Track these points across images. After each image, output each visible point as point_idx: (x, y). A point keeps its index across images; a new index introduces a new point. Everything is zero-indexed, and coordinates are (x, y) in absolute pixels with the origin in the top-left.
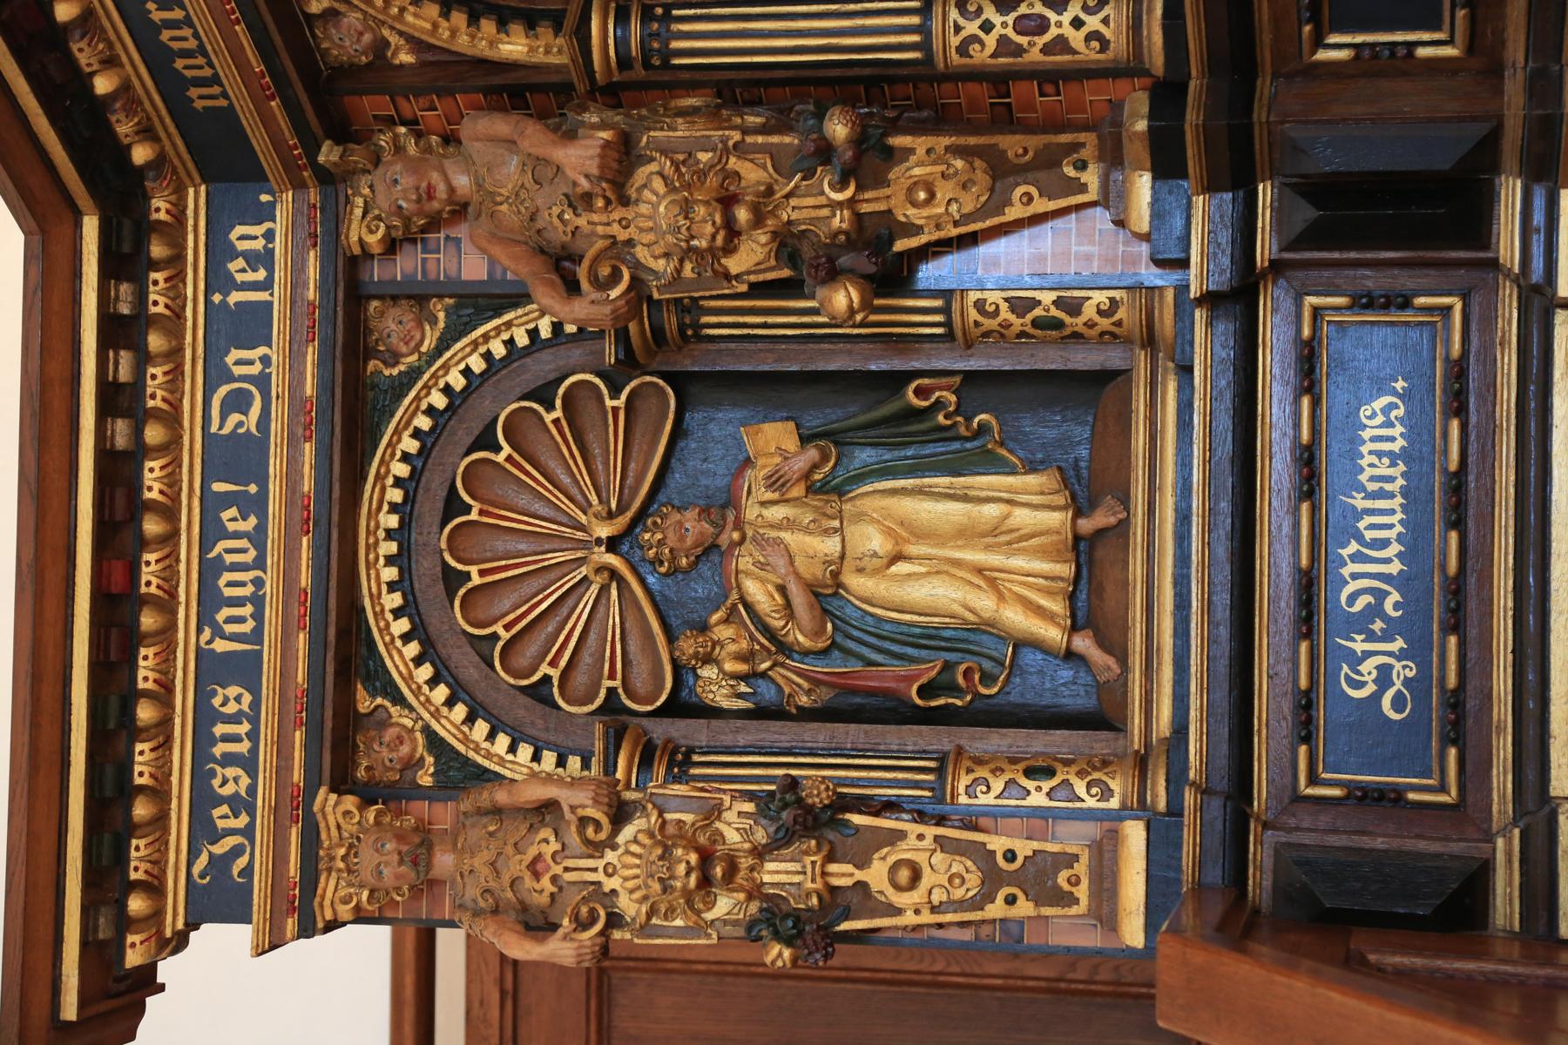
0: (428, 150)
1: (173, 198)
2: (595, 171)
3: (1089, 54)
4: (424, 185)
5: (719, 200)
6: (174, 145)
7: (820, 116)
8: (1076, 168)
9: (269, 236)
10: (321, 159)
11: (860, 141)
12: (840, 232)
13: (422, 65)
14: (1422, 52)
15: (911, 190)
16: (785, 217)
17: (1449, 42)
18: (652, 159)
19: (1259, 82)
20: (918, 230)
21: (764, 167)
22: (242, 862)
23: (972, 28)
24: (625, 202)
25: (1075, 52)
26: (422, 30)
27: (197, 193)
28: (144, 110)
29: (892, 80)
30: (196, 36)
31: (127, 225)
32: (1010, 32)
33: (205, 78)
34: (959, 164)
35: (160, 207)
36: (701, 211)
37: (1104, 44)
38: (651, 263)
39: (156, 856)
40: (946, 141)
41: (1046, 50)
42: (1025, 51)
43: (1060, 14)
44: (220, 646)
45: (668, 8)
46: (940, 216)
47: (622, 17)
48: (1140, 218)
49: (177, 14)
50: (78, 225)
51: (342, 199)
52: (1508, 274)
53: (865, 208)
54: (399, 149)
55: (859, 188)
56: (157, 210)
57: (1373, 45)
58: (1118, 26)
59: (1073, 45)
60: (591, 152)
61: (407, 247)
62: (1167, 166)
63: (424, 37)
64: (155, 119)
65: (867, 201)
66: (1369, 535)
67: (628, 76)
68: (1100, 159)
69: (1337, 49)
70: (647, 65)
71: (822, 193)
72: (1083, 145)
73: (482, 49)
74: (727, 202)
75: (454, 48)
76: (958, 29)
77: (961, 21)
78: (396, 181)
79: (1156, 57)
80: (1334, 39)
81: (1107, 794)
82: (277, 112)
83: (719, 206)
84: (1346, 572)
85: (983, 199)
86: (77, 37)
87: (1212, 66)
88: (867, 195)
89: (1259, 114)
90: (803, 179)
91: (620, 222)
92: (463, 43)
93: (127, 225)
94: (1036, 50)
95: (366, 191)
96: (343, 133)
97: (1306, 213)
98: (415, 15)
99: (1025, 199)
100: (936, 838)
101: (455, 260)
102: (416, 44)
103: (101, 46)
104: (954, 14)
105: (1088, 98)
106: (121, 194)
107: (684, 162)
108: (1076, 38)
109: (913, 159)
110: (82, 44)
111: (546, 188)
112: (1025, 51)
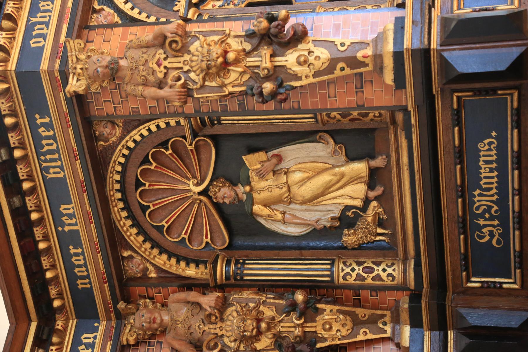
0: (156, 307)
1: (64, 322)
2: (213, 305)
3: (388, 282)
4: (152, 317)
5: (256, 319)
6: (69, 302)
7: (293, 294)
8: (383, 325)
9: (95, 338)
10: (118, 306)
11: (306, 302)
12: (297, 336)
13: (158, 278)
14: (505, 286)
15: (324, 325)
16: (278, 330)
17: (515, 283)
18: (234, 305)
19: (448, 293)
20: (325, 340)
21: (273, 311)
23: (348, 270)
24: (222, 320)
25: (383, 281)
26: (160, 264)
27: (73, 322)
28: (61, 287)
29: (319, 287)
30: (84, 259)
31: (47, 329)
32: (361, 272)
33: (84, 276)
34: (341, 317)
35: (59, 324)
36: (249, 322)
37: (394, 278)
38: (229, 344)
40: (336, 308)
41: (373, 279)
42: (366, 279)
43: (378, 267)
45: (244, 260)
46: (334, 335)
47: (228, 263)
48: (406, 341)
49: (79, 251)
50: (29, 325)
51: (123, 325)
53: (307, 330)
54: (146, 306)
55: (305, 322)
56: (58, 325)
57: (487, 282)
58: (398, 271)
59: (383, 278)
60: (212, 299)
61: (143, 344)
62: (416, 323)
63: (161, 266)
64: (64, 291)
65: (308, 327)
66: (484, 186)
67: (228, 282)
68: (392, 322)
69: (475, 283)
70: (235, 279)
71: (293, 322)
72: (385, 316)
73: (180, 272)
74: (259, 321)
75: (170, 271)
76: (343, 270)
77: (344, 268)
78: (143, 316)
79: (412, 284)
80: (474, 279)
82: (106, 288)
83: (255, 320)
84: (476, 199)
85: (349, 332)
86: (45, 254)
87: (432, 285)
88: (309, 325)
89: (448, 303)
90: (286, 316)
91: (220, 328)
92: (173, 270)
93: (47, 329)
94: (370, 279)
95: (132, 321)
96: (128, 301)
97: (466, 341)
98: (159, 258)
99: (364, 334)
101: (159, 349)
102: (158, 269)
103: (51, 260)
104: (342, 265)
105: (388, 298)
106: (47, 315)
107: (244, 307)
108: (384, 275)
109: (325, 313)
110: (45, 258)
111: (195, 317)
112: (366, 279)
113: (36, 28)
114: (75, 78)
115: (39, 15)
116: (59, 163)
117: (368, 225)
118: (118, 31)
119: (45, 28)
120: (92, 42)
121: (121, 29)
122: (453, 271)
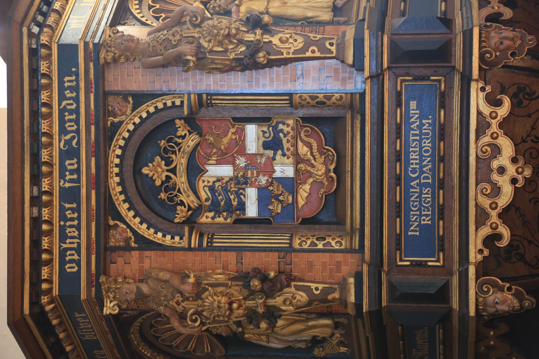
22: (75, 141)
39: (50, 213)
44: (67, 185)
52: (458, 71)
81: (341, 245)
100: (282, 54)
113: (68, 253)
114: (108, 301)
115: (68, 241)
116: (94, 333)
117: (333, 346)
118: (135, 254)
119: (76, 255)
120: (115, 263)
121: (137, 252)
122: (389, 251)
